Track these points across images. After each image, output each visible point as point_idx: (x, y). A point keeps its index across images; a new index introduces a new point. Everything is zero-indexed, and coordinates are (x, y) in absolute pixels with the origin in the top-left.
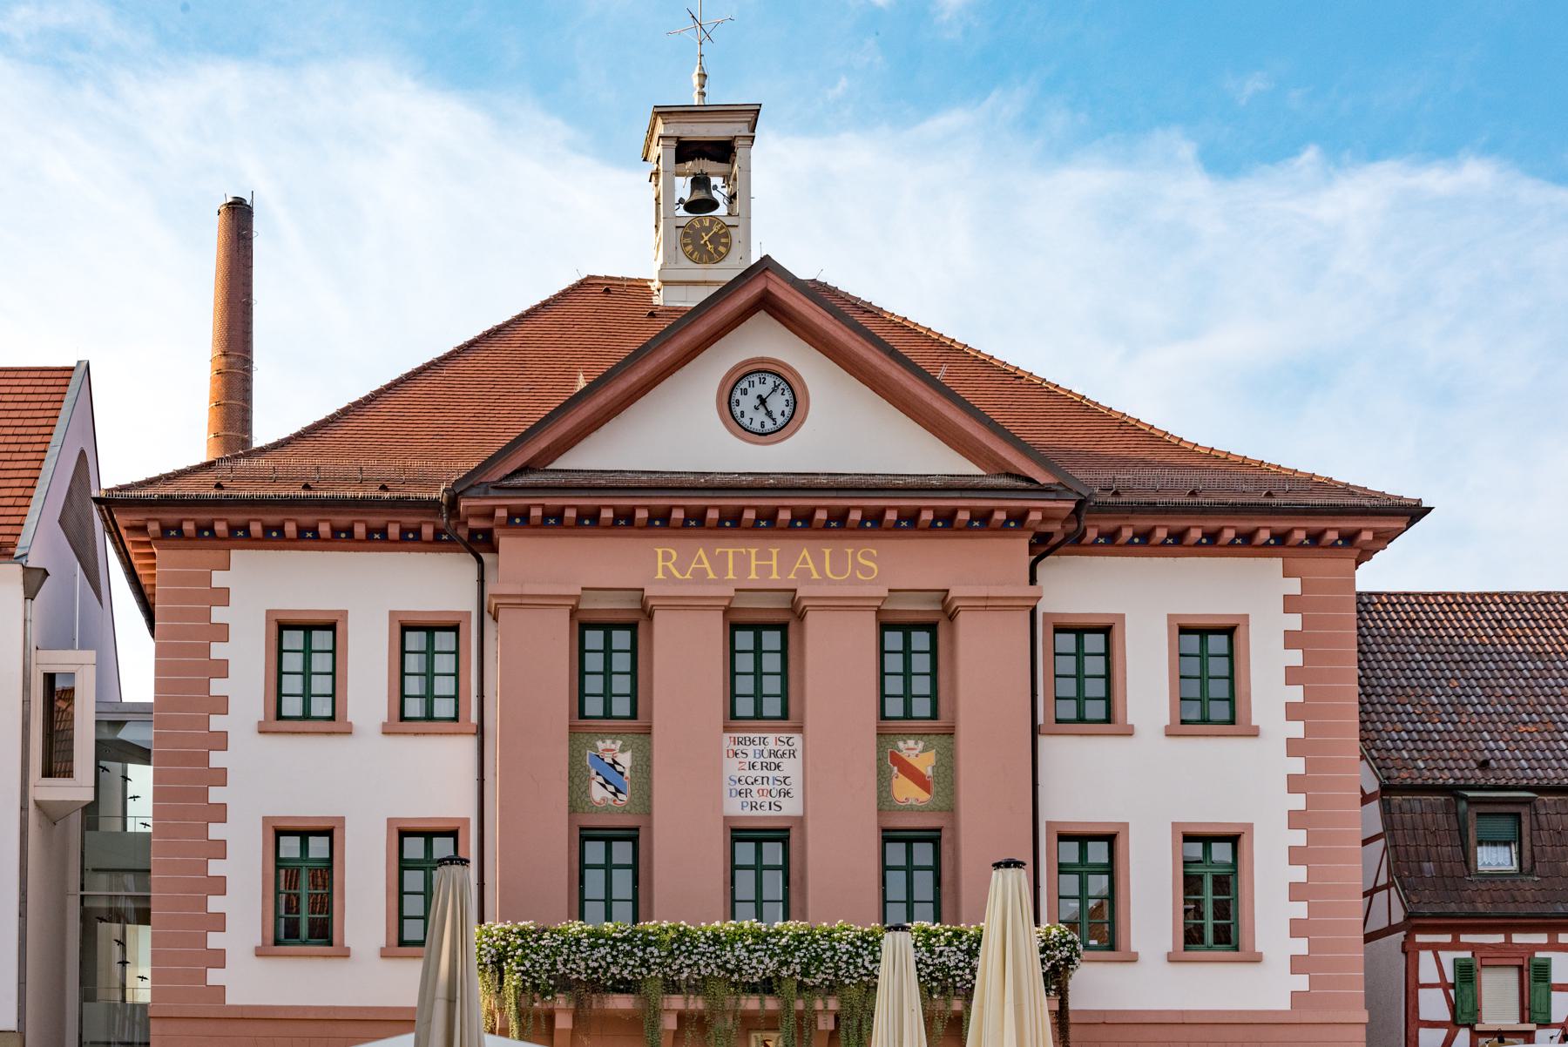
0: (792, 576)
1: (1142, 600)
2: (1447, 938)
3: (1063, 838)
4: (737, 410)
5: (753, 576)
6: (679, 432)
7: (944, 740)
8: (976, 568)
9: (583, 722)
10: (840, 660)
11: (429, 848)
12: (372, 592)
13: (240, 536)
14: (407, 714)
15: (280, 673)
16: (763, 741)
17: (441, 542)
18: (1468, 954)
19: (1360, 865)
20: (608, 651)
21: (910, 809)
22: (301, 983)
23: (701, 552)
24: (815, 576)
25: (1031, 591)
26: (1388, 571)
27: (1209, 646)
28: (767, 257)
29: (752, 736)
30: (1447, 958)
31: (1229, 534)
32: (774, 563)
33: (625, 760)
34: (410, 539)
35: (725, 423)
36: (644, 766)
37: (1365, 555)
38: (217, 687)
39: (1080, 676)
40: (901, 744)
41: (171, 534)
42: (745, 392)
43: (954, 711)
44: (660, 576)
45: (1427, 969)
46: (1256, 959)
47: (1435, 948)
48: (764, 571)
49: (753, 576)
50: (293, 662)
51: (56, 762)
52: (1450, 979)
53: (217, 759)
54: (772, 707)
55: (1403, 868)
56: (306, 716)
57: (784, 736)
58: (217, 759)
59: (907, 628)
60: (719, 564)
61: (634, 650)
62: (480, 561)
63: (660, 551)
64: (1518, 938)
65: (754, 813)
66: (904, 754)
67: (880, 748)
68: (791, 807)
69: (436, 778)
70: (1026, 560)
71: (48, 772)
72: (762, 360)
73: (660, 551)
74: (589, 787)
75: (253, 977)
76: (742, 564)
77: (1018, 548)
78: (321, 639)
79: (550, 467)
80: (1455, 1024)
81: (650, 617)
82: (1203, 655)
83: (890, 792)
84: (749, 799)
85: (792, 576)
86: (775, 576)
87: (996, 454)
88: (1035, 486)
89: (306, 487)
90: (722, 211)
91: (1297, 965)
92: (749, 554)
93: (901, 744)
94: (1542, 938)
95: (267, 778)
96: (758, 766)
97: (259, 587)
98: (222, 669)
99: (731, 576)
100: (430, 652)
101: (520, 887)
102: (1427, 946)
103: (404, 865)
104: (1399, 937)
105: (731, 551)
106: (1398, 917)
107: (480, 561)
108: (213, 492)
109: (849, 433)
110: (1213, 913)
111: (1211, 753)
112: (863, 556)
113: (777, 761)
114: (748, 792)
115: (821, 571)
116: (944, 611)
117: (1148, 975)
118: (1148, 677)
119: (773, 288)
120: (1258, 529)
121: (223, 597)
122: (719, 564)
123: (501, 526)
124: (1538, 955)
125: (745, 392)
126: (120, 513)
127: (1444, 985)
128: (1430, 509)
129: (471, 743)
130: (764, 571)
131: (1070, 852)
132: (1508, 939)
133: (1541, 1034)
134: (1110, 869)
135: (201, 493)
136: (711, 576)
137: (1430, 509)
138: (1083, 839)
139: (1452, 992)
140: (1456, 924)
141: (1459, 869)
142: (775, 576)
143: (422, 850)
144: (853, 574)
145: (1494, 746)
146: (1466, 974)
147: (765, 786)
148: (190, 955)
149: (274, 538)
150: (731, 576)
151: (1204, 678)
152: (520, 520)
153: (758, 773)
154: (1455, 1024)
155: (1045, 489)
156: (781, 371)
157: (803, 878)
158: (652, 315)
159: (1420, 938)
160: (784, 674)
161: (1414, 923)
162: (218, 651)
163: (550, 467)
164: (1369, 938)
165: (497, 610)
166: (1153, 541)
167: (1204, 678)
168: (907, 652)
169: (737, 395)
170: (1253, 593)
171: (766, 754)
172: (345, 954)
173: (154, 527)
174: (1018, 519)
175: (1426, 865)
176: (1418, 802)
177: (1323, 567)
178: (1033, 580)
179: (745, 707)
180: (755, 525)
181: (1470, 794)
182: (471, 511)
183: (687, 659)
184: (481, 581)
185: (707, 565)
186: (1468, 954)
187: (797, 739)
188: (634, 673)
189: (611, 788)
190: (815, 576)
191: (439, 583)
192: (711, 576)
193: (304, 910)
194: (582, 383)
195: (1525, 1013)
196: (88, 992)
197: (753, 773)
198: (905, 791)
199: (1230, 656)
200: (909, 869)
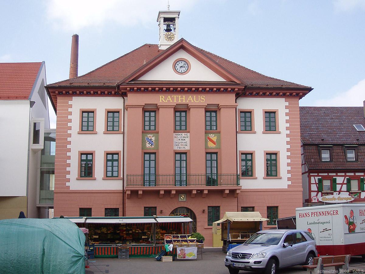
1: (258, 106)
2: (316, 174)
3: (242, 154)
4: (176, 68)
6: (165, 73)
7: (156, 134)
8: (228, 99)
9: (145, 131)
10: (197, 118)
11: (87, 157)
12: (101, 105)
13: (75, 94)
14: (118, 130)
15: (176, 121)
17: (116, 94)
18: (321, 177)
19: (299, 160)
20: (150, 116)
21: (211, 148)
22: (86, 185)
25: (234, 104)
26: (305, 102)
27: (270, 116)
28: (182, 38)
29: (179, 134)
30: (317, 178)
31: (274, 93)
32: (184, 99)
33: (153, 139)
34: (109, 94)
36: (157, 140)
37: (301, 98)
38: (69, 124)
39: (113, 122)
41: (61, 94)
42: (178, 65)
43: (158, 129)
44: (161, 101)
45: (313, 181)
46: (281, 178)
47: (314, 176)
51: (36, 140)
52: (317, 182)
54: (183, 128)
55: (307, 160)
57: (186, 134)
59: (211, 112)
60: (173, 99)
61: (155, 117)
62: (124, 98)
63: (161, 96)
64: (330, 174)
66: (210, 137)
67: (205, 136)
68: (187, 148)
69: (114, 142)
70: (235, 98)
71: (34, 143)
72: (181, 59)
75: (76, 184)
77: (233, 96)
80: (318, 192)
81: (159, 109)
82: (245, 117)
83: (207, 145)
84: (179, 146)
86: (184, 101)
87: (229, 77)
88: (236, 83)
89: (88, 84)
90: (173, 31)
91: (289, 179)
94: (335, 174)
95: (79, 143)
97: (78, 104)
98: (70, 121)
101: (132, 166)
102: (312, 176)
103: (108, 160)
104: (307, 174)
106: (307, 170)
107: (124, 98)
108: (69, 85)
109: (200, 73)
110: (272, 169)
111: (271, 137)
115: (193, 100)
116: (218, 108)
118: (259, 121)
119: (183, 44)
120: (266, 92)
121: (71, 106)
122: (173, 99)
123: (128, 91)
124: (334, 177)
125: (178, 65)
126: (50, 89)
127: (316, 183)
128: (313, 89)
129: (122, 135)
131: (244, 157)
132: (355, 174)
133: (335, 193)
134: (251, 160)
135: (67, 85)
136: (171, 101)
137: (313, 89)
138: (246, 154)
139: (317, 185)
140: (318, 171)
141: (319, 160)
143: (111, 157)
144: (200, 101)
145: (325, 136)
146: (320, 181)
148: (63, 180)
149: (81, 94)
151: (245, 121)
152: (132, 90)
154: (318, 192)
155: (239, 84)
157: (221, 164)
158: (159, 51)
159: (311, 174)
160: (186, 121)
161: (310, 171)
164: (303, 174)
165: (127, 108)
166: (260, 95)
167: (245, 121)
168: (211, 117)
169: (176, 65)
170: (279, 105)
173: (57, 92)
174: (233, 90)
175: (312, 160)
176: (311, 148)
177: (293, 100)
178: (236, 102)
179: (178, 128)
180: (194, 91)
181: (320, 146)
182: (122, 88)
183: (166, 118)
184: (124, 103)
186: (321, 177)
187: (189, 134)
188: (155, 121)
190: (192, 101)
193: (87, 171)
194: (145, 63)
195: (359, 189)
196: (42, 188)
198: (210, 145)
199: (251, 117)
200: (211, 160)
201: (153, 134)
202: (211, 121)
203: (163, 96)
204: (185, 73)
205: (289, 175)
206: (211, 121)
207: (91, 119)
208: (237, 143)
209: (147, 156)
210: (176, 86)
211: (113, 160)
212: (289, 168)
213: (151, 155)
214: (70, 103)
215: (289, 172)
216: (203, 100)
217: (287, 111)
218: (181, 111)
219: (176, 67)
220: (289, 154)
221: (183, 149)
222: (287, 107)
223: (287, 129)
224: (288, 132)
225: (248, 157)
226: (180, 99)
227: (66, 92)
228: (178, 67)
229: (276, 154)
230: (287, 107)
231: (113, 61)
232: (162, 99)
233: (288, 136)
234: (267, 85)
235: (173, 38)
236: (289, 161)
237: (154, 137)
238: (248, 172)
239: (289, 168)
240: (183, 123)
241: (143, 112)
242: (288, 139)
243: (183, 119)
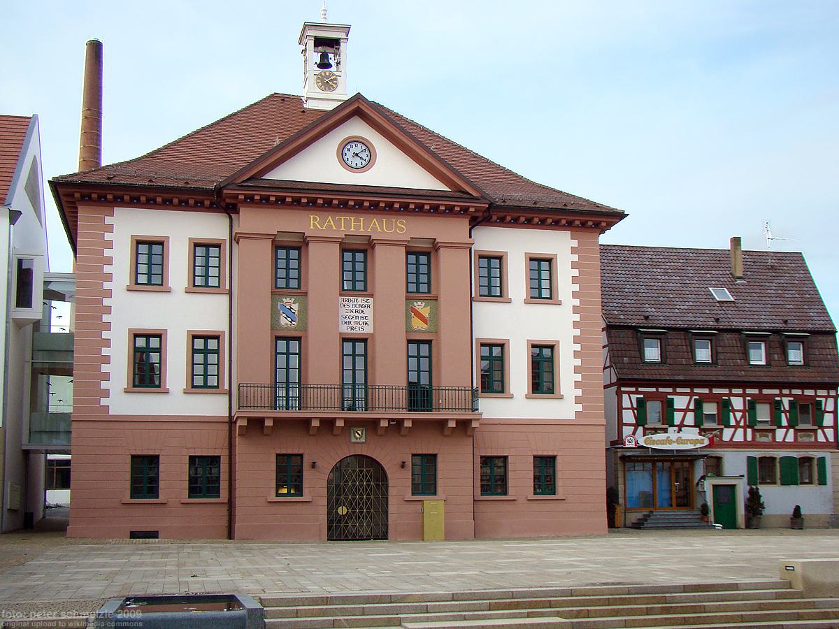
1: (516, 246)
2: (634, 389)
4: (346, 158)
6: (319, 166)
8: (449, 230)
16: (356, 300)
27: (541, 265)
29: (351, 298)
30: (634, 397)
33: (295, 307)
42: (349, 150)
44: (312, 227)
48: (357, 227)
60: (338, 224)
66: (417, 308)
68: (368, 329)
74: (279, 319)
84: (350, 326)
95: (130, 311)
113: (362, 309)
115: (382, 228)
118: (517, 278)
119: (361, 107)
121: (110, 228)
125: (349, 150)
130: (357, 227)
156: (358, 140)
170: (559, 245)
171: (357, 306)
191: (212, 227)
202: (418, 274)
204: (357, 169)
207: (156, 259)
210: (407, 201)
214: (108, 220)
222: (574, 250)
228: (349, 155)
230: (574, 250)
232: (314, 224)
237: (297, 304)
240: (294, 274)
243: (294, 264)
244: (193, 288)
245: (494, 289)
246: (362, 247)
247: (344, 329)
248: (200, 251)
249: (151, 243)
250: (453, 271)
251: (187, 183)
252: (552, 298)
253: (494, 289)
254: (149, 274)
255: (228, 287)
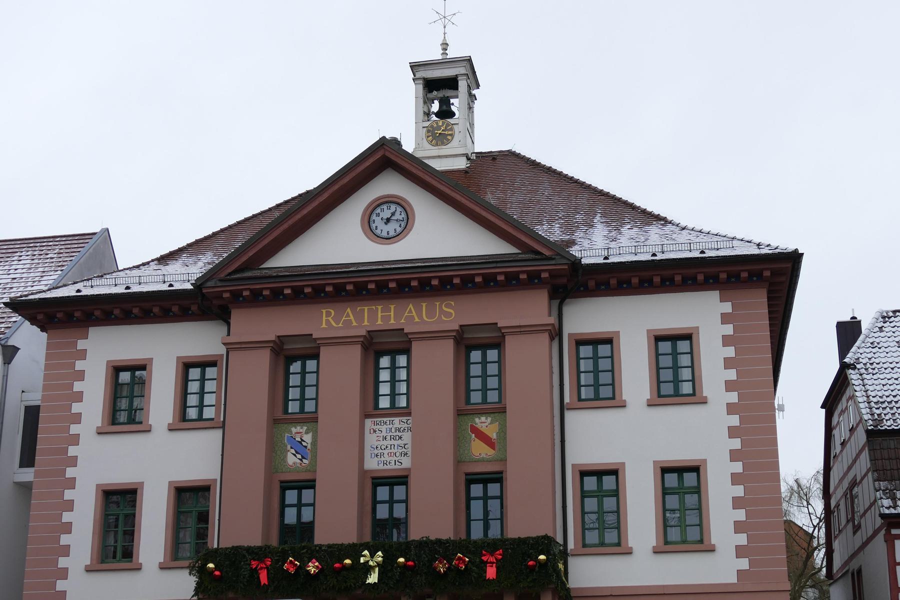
0: (403, 321)
1: (631, 322)
4: (373, 226)
5: (379, 322)
6: (339, 243)
8: (533, 308)
16: (392, 423)
20: (484, 363)
21: (483, 461)
23: (349, 310)
24: (417, 320)
27: (672, 346)
28: (383, 143)
29: (385, 419)
32: (392, 313)
33: (308, 438)
35: (365, 234)
40: (477, 420)
42: (378, 215)
44: (324, 326)
48: (386, 319)
49: (379, 322)
50: (194, 387)
53: (72, 451)
56: (200, 418)
58: (72, 451)
60: (359, 317)
63: (324, 311)
65: (386, 467)
66: (479, 426)
68: (406, 463)
73: (324, 311)
74: (286, 456)
75: (643, 565)
76: (373, 316)
78: (683, 346)
79: (262, 266)
84: (383, 459)
85: (403, 321)
86: (392, 321)
91: (740, 552)
92: (377, 309)
93: (477, 420)
95: (99, 460)
96: (388, 438)
97: (105, 347)
98: (79, 397)
99: (366, 323)
100: (675, 354)
105: (366, 308)
111: (120, 477)
112: (446, 306)
113: (400, 434)
114: (382, 455)
115: (420, 316)
117: (643, 565)
118: (635, 371)
119: (388, 154)
121: (83, 355)
125: (378, 215)
130: (386, 319)
134: (616, 493)
136: (355, 324)
142: (392, 321)
147: (393, 450)
150: (366, 323)
153: (388, 442)
156: (390, 199)
162: (78, 386)
163: (262, 266)
171: (393, 430)
172: (139, 568)
183: (340, 370)
185: (352, 317)
189: (299, 456)
190: (417, 320)
191: (201, 339)
192: (355, 324)
197: (385, 443)
201: (492, 415)
202: (596, 371)
203: (332, 312)
204: (389, 239)
205: (742, 539)
206: (596, 371)
207: (604, 364)
208: (222, 455)
209: (477, 490)
210: (258, 287)
211: (600, 494)
212: (741, 515)
213: (685, 475)
214: (81, 344)
215: (739, 527)
216: (448, 314)
217: (729, 329)
218: (377, 346)
219: (371, 223)
220: (738, 467)
221: (394, 467)
223: (730, 386)
224: (733, 397)
225: (603, 481)
226: (380, 314)
227: (596, 284)
228: (378, 223)
229: (614, 472)
230: (725, 319)
231: (254, 216)
232: (327, 321)
233: (731, 409)
234: (606, 258)
235: (449, 137)
236: (739, 491)
237: (310, 435)
238: (608, 535)
239: (741, 515)
240: (493, 383)
241: (463, 349)
242: (735, 420)
243: (492, 369)
244: (183, 420)
245: (604, 393)
246: (401, 346)
247: (372, 464)
248: (665, 347)
249: (674, 338)
250: (527, 365)
251: (171, 285)
252: (696, 398)
253: (604, 393)
254: (596, 385)
255: (222, 419)
